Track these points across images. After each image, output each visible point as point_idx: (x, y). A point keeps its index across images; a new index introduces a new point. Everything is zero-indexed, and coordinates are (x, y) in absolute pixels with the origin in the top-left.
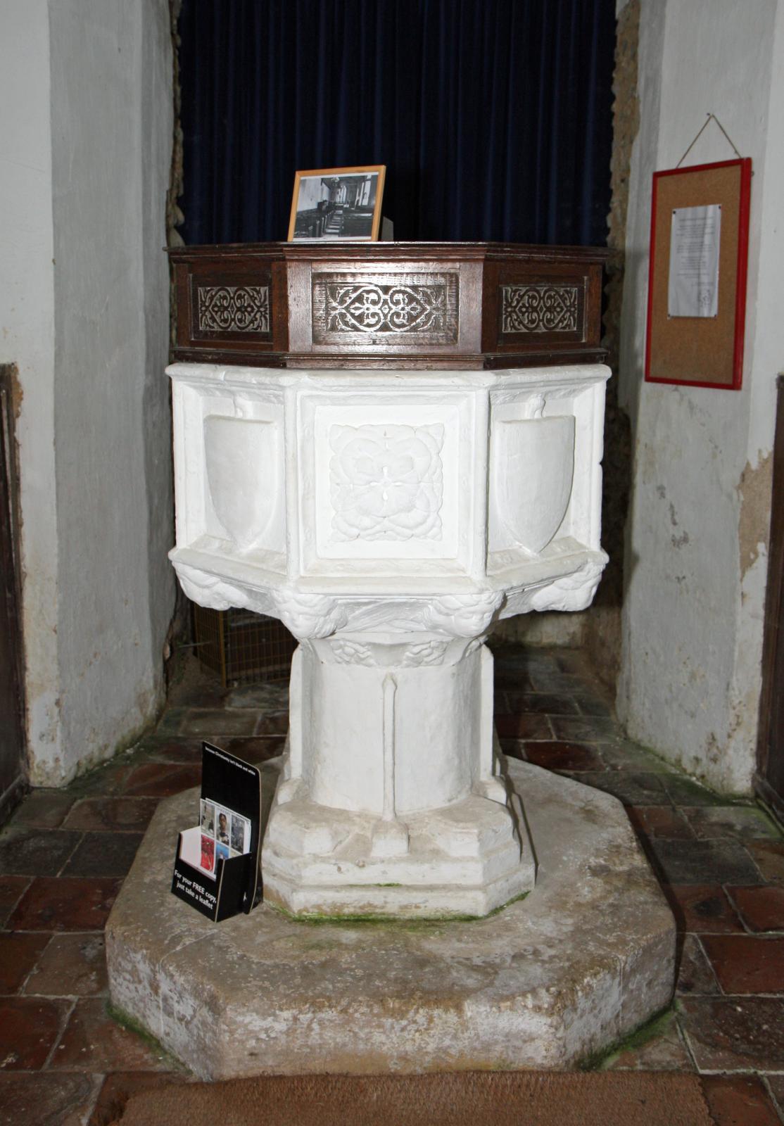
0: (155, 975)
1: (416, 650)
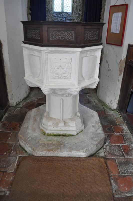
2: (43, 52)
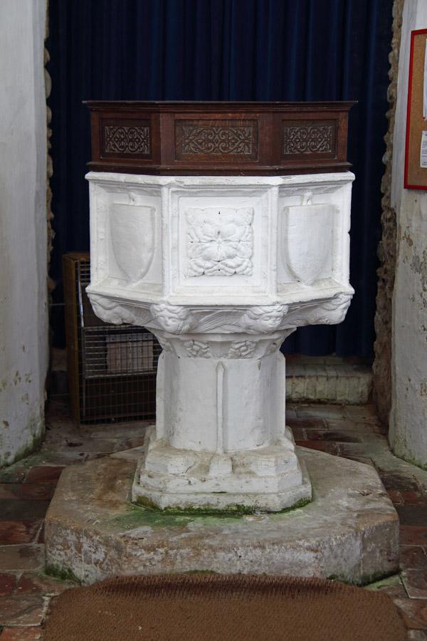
0: (79, 540)
1: (237, 346)
2: (165, 190)
